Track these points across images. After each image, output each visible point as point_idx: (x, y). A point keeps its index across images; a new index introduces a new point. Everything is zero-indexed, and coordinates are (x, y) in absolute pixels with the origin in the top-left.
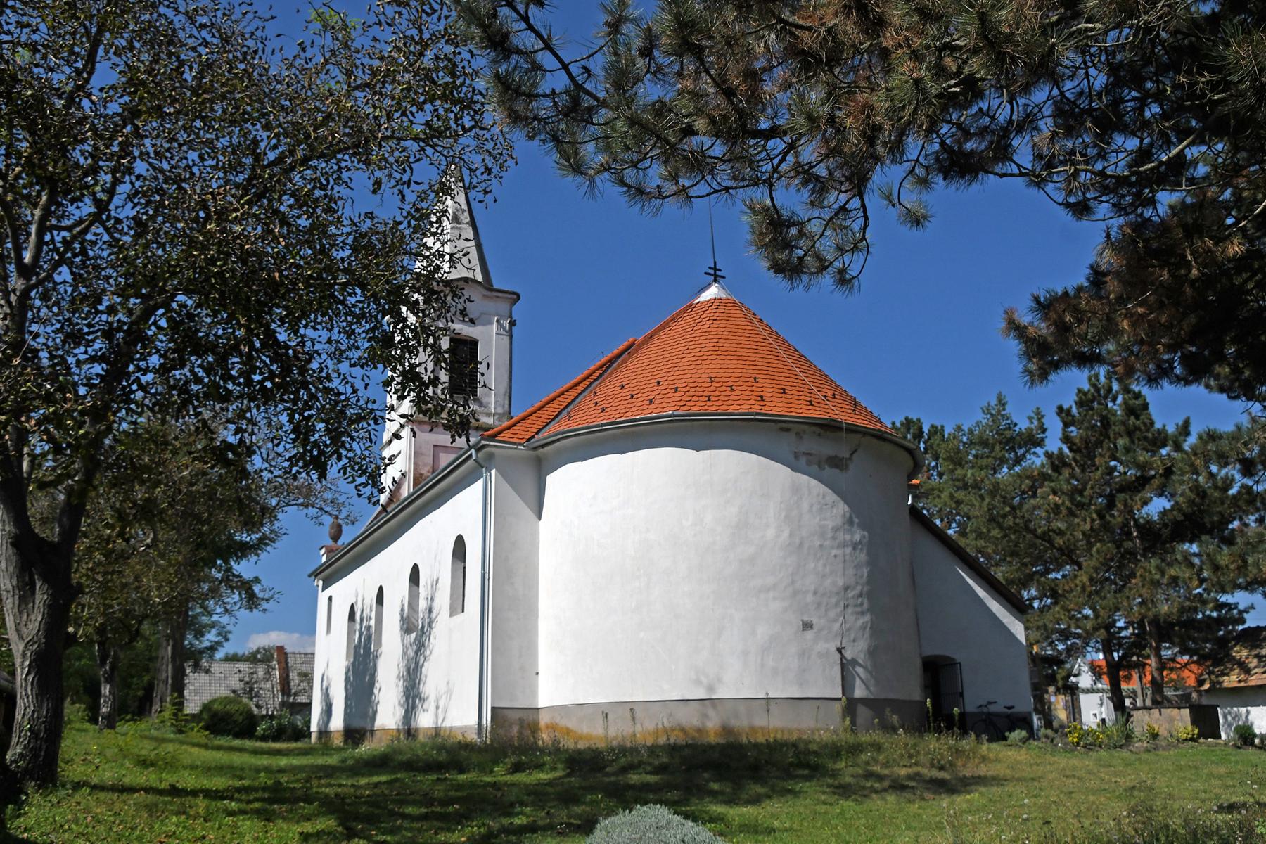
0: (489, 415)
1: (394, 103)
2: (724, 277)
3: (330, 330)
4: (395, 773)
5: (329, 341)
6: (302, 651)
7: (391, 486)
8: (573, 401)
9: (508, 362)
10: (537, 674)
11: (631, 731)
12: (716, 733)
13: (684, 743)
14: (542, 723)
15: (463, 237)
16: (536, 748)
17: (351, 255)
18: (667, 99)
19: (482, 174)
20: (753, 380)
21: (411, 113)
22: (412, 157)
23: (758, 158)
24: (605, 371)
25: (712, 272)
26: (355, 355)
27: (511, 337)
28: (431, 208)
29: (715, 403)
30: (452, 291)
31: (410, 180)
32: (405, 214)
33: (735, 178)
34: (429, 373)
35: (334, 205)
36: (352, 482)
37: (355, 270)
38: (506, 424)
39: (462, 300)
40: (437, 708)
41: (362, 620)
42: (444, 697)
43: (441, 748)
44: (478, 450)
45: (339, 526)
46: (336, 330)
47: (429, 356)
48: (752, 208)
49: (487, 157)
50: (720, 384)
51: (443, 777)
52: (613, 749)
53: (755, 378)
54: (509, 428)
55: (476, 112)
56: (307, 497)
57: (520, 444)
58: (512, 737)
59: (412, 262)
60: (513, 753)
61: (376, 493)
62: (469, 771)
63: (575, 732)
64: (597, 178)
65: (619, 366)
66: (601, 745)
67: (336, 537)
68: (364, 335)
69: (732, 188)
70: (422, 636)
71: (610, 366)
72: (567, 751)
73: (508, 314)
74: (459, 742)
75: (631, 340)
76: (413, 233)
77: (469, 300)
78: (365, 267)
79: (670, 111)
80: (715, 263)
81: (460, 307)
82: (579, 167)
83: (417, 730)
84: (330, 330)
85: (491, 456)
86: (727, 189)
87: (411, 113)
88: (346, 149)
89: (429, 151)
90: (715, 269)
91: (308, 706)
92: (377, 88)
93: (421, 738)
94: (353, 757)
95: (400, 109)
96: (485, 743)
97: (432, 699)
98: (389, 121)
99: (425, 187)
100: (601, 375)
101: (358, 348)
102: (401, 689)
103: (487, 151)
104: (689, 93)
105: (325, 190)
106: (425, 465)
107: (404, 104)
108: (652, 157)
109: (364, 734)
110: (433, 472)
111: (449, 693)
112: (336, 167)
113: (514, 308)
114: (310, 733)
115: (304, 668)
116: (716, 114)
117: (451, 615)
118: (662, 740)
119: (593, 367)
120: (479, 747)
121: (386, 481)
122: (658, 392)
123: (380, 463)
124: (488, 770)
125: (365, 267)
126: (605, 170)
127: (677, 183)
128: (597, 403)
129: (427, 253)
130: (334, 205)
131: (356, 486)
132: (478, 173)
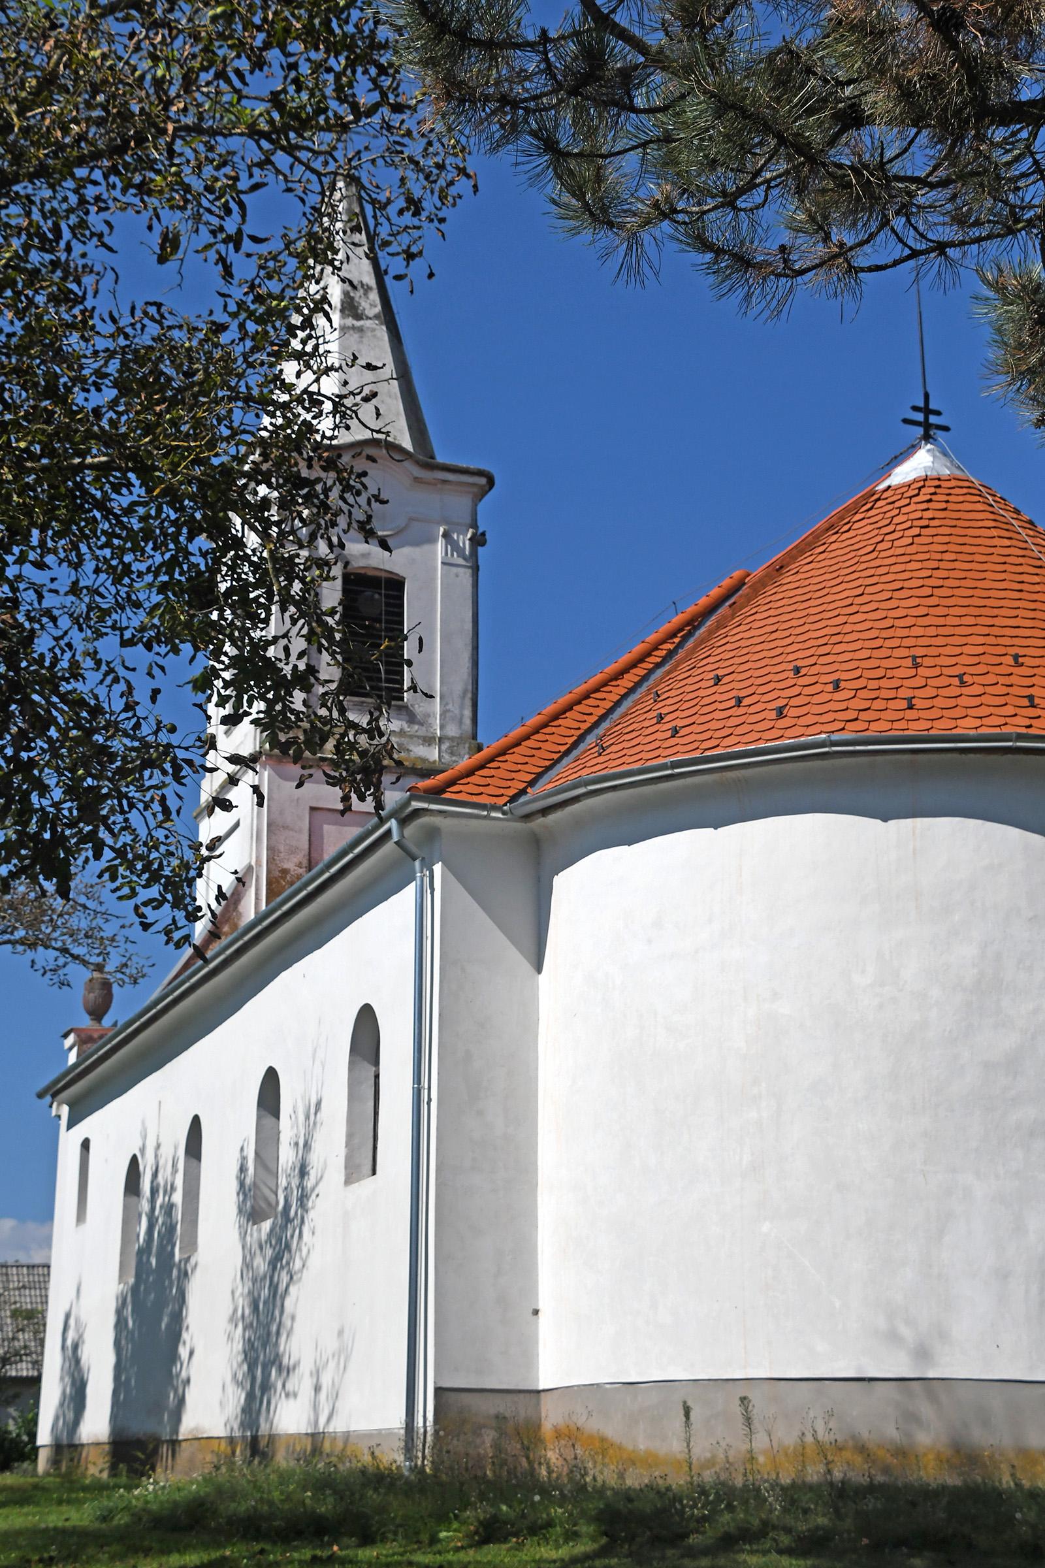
0: (428, 741)
1: (196, 49)
2: (946, 429)
3: (77, 565)
4: (220, 1546)
5: (75, 589)
6: (24, 1260)
7: (214, 905)
8: (610, 711)
9: (469, 626)
10: (536, 1312)
11: (747, 1447)
12: (939, 1458)
13: (865, 1481)
14: (547, 1427)
15: (362, 361)
16: (537, 1486)
17: (114, 403)
18: (801, 45)
19: (401, 212)
20: (1011, 661)
21: (238, 73)
22: (244, 176)
23: (1015, 172)
24: (679, 646)
25: (920, 417)
26: (134, 619)
27: (476, 569)
28: (289, 293)
29: (922, 714)
30: (340, 480)
31: (240, 232)
32: (232, 308)
33: (960, 220)
34: (293, 659)
35: (74, 287)
36: (129, 897)
37: (125, 436)
38: (465, 761)
39: (362, 500)
40: (317, 1389)
41: (154, 1191)
42: (332, 1365)
43: (324, 1484)
44: (403, 822)
45: (106, 986)
46: (89, 566)
47: (294, 622)
48: (999, 288)
49: (411, 175)
50: (937, 671)
51: (325, 1554)
52: (704, 1492)
53: (1016, 657)
54: (470, 772)
55: (383, 71)
56: (32, 925)
57: (495, 808)
58: (480, 1458)
59: (250, 418)
60: (482, 1497)
61: (182, 922)
62: (384, 1539)
63: (620, 1448)
64: (645, 236)
65: (711, 632)
66: (678, 1481)
67: (98, 1012)
68: (149, 578)
69: (952, 244)
70: (284, 1228)
71: (690, 634)
72: (600, 1492)
73: (468, 520)
74: (363, 1472)
75: (737, 574)
76: (253, 350)
77: (377, 498)
78: (148, 429)
79: (809, 71)
80: (927, 397)
81: (359, 515)
82: (604, 210)
83: (272, 1438)
84: (77, 565)
85: (432, 834)
86: (941, 247)
87: (238, 73)
88: (97, 155)
89: (281, 159)
90: (927, 411)
91: (36, 1382)
92: (159, 13)
93: (282, 1459)
94: (127, 1508)
95: (212, 63)
96: (422, 1470)
97: (306, 1368)
98: (187, 91)
99: (276, 245)
100: (671, 654)
101: (137, 605)
102: (238, 1346)
103: (411, 160)
104: (853, 28)
105: (51, 251)
106: (293, 851)
107: (220, 52)
108: (768, 181)
109: (155, 1451)
110: (310, 869)
111: (343, 1355)
112: (73, 199)
113: (481, 506)
114: (35, 1450)
115: (26, 1301)
116: (912, 73)
117: (348, 1181)
118: (814, 1473)
119: (652, 638)
120: (407, 1482)
121: (204, 894)
122: (796, 691)
123: (189, 855)
124: (425, 1537)
125: (148, 429)
126: (664, 215)
127: (827, 238)
128: (661, 717)
129: (285, 398)
130: (74, 287)
131: (136, 908)
132: (392, 210)
